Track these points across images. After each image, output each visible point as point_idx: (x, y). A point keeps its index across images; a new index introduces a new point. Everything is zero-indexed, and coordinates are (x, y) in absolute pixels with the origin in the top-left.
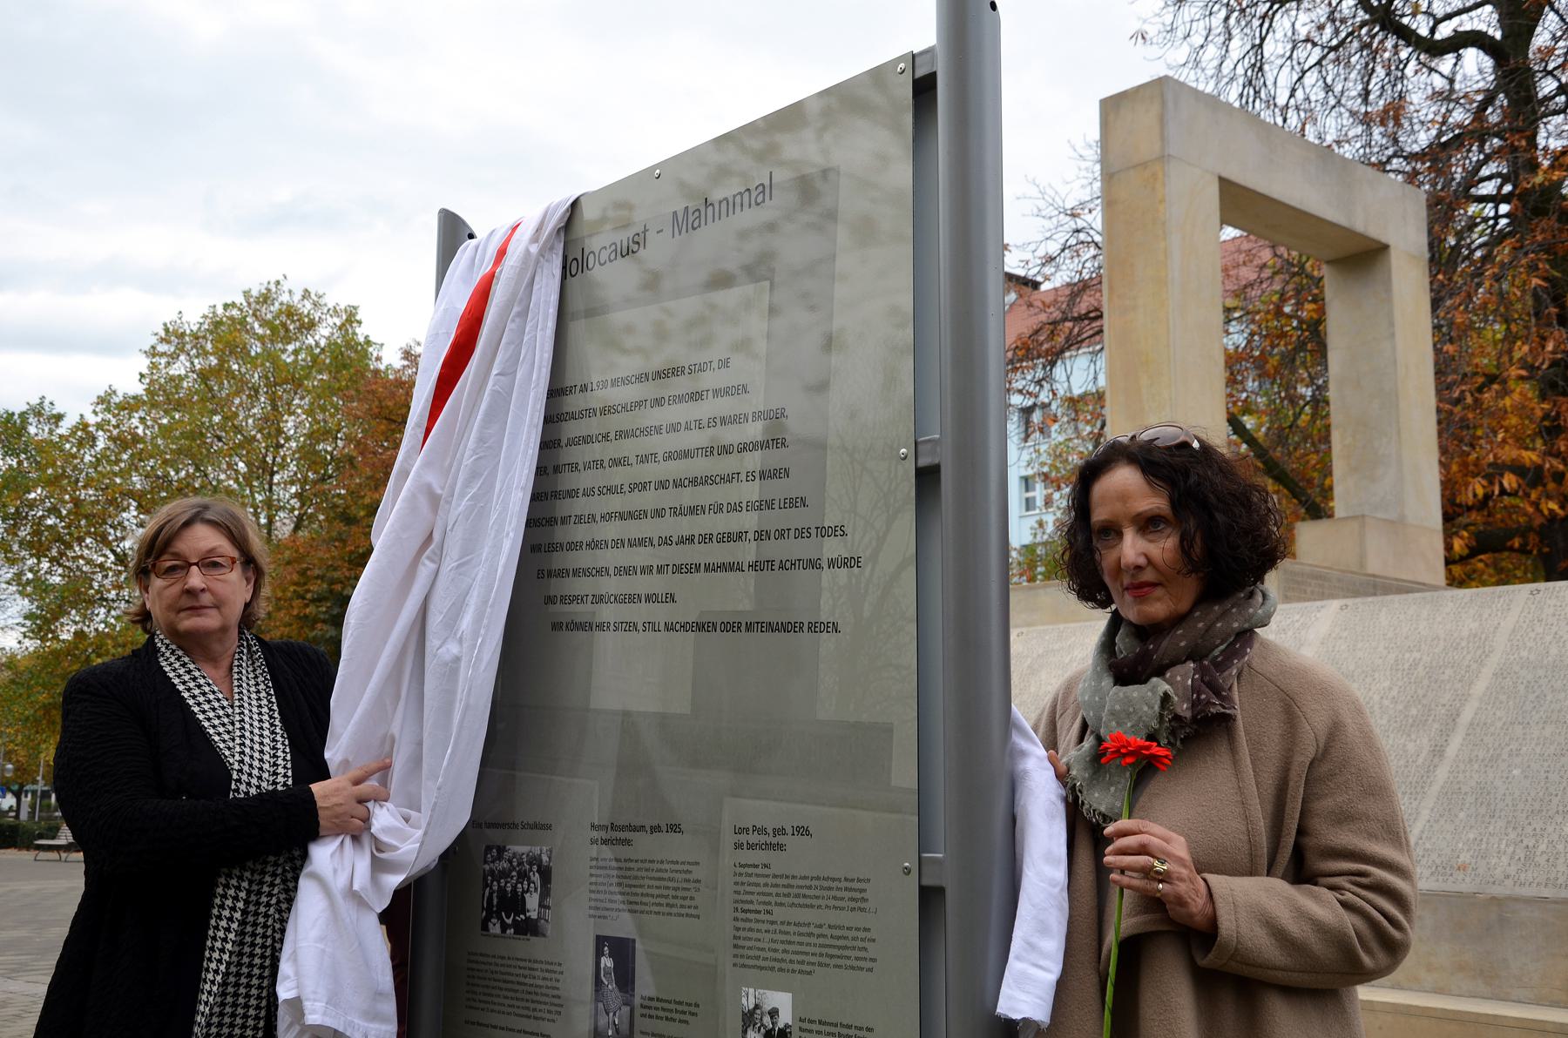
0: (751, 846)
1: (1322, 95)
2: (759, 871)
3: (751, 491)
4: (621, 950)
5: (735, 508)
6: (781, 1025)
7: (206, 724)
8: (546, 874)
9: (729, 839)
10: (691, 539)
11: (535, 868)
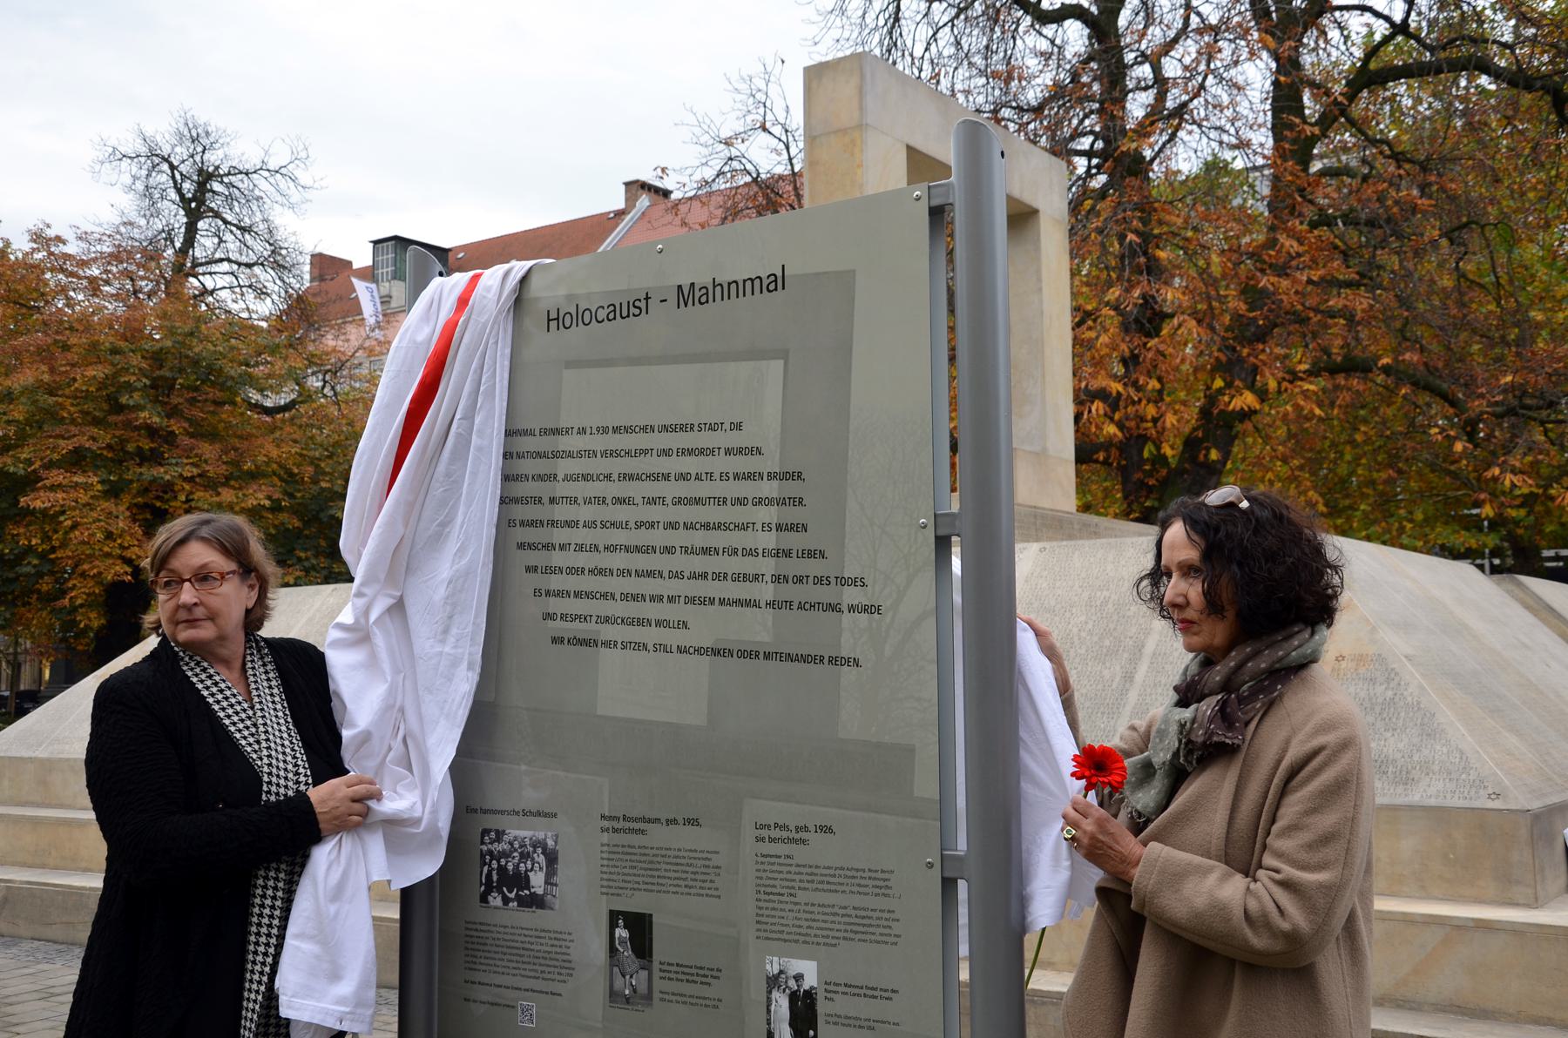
0: (772, 840)
1: (952, 50)
2: (782, 860)
3: (769, 540)
4: (640, 927)
5: (752, 553)
6: (806, 986)
7: (232, 729)
8: (552, 859)
9: (749, 833)
10: (704, 576)
11: (539, 850)
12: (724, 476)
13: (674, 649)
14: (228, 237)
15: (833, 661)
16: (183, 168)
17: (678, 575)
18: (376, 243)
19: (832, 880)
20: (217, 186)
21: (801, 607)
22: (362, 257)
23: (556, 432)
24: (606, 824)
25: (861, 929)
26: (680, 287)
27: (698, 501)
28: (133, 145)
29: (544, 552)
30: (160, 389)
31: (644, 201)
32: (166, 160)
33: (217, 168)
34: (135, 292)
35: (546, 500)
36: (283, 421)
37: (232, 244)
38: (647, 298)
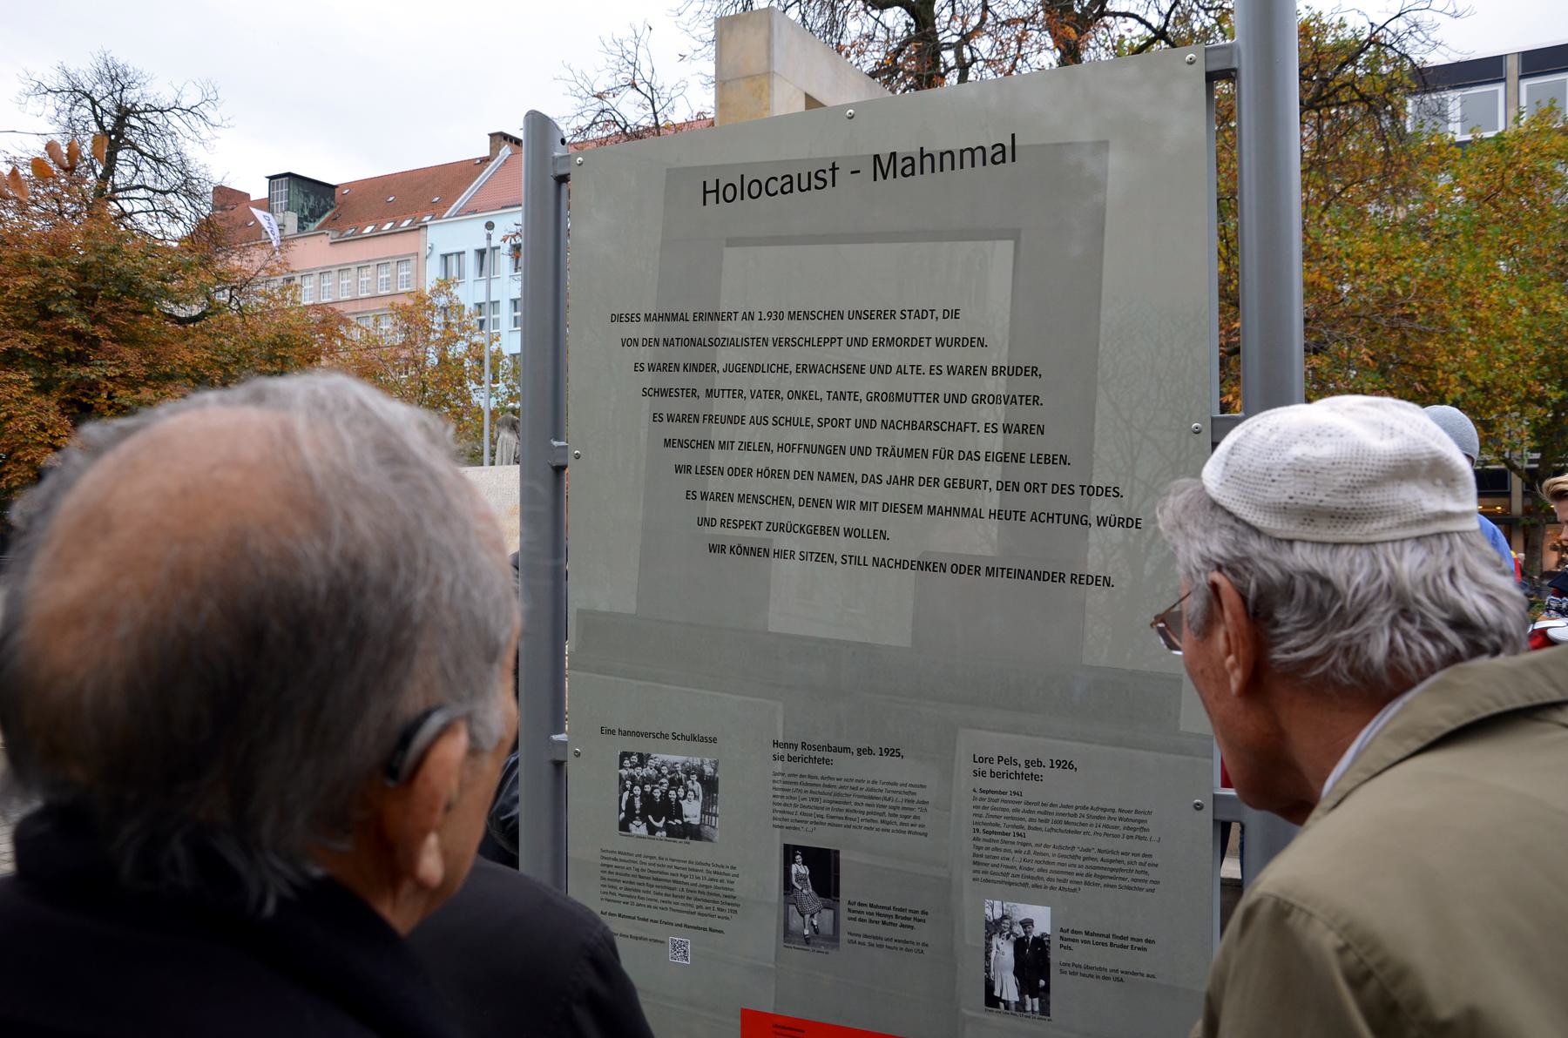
0: (994, 774)
3: (996, 442)
5: (972, 456)
6: (1036, 932)
8: (710, 785)
9: (964, 767)
10: (909, 481)
11: (694, 777)
12: (935, 370)
13: (869, 561)
14: (144, 166)
15: (1077, 579)
16: (103, 104)
17: (875, 479)
18: (271, 178)
19: (1071, 820)
20: (133, 121)
21: (1035, 517)
22: (259, 191)
23: (716, 316)
24: (780, 751)
25: (1108, 873)
26: (877, 157)
27: (900, 397)
28: (56, 80)
29: (700, 451)
30: (85, 298)
31: (506, 150)
32: (87, 95)
33: (134, 105)
34: (61, 213)
35: (701, 392)
36: (195, 330)
37: (148, 175)
38: (834, 169)
